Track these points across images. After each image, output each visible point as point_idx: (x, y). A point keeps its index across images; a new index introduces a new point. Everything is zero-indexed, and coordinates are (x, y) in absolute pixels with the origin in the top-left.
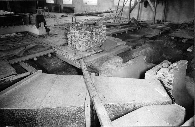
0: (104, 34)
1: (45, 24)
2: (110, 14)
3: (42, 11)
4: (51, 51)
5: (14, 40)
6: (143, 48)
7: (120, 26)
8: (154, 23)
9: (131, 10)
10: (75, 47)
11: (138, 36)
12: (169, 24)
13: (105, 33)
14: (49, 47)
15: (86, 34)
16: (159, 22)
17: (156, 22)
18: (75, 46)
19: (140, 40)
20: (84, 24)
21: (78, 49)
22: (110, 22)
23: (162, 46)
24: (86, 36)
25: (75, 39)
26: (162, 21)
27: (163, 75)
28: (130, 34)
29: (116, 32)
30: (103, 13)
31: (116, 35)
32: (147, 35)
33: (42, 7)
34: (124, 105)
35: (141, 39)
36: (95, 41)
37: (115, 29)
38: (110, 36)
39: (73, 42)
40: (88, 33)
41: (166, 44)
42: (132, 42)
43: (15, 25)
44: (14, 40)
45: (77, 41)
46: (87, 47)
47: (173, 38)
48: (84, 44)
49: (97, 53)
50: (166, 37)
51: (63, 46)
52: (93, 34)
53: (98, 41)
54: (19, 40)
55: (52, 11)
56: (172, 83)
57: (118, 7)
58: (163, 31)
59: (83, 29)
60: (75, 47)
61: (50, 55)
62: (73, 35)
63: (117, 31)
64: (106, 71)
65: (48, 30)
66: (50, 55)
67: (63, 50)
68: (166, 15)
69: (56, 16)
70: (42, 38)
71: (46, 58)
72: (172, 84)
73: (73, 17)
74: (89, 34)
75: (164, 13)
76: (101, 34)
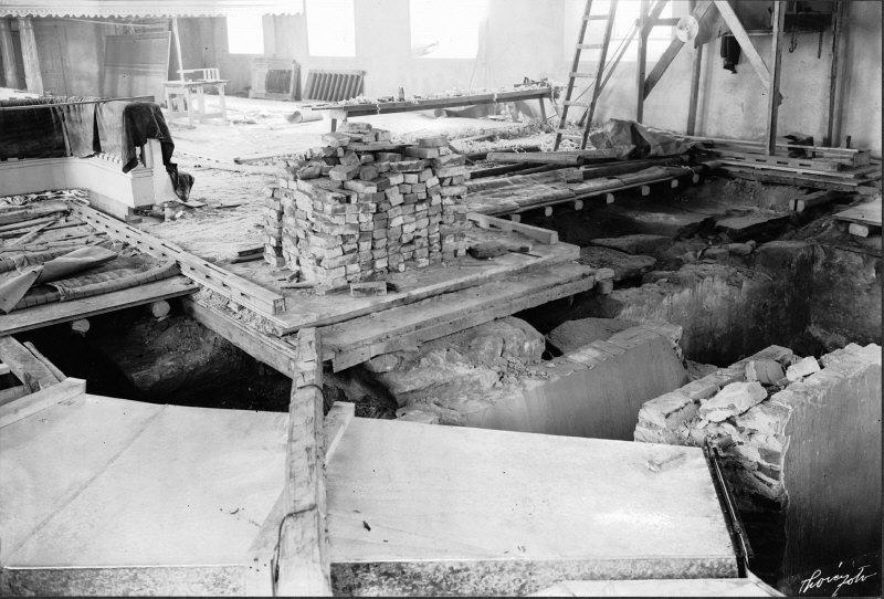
0: (451, 202)
1: (167, 149)
2: (542, 103)
3: (187, 90)
4: (175, 286)
5: (10, 230)
6: (678, 283)
7: (577, 166)
8: (772, 154)
9: (646, 87)
10: (298, 268)
11: (673, 219)
12: (852, 160)
13: (459, 197)
14: (165, 267)
15: (348, 200)
16: (800, 147)
17: (783, 144)
18: (298, 262)
19: (678, 244)
20: (345, 149)
21: (310, 276)
22: (535, 149)
23: (798, 274)
24: (350, 208)
25: (297, 226)
26: (818, 138)
27: (730, 420)
28: (631, 208)
29: (546, 200)
30: (498, 100)
31: (549, 212)
32: (728, 215)
33: (192, 71)
34: (460, 575)
35: (691, 236)
36: (400, 240)
37: (549, 179)
38: (514, 217)
39: (286, 242)
40: (362, 196)
41: (824, 265)
42: (637, 253)
43: (22, 156)
44: (10, 230)
45: (306, 235)
46: (355, 267)
47: (862, 231)
48: (339, 251)
49: (404, 302)
50: (826, 227)
51: (238, 262)
52: (391, 199)
53: (419, 237)
54: (36, 229)
55: (251, 93)
56: (781, 467)
57: (575, 69)
58: (813, 196)
59: (337, 174)
60: (298, 268)
61: (161, 311)
62: (287, 202)
63: (560, 190)
64: (436, 399)
65: (182, 183)
66: (161, 311)
67: (226, 281)
68: (841, 111)
69: (264, 116)
70: (148, 223)
71: (143, 326)
72: (782, 475)
73: (334, 122)
74: (367, 198)
75: (828, 101)
76: (436, 199)
